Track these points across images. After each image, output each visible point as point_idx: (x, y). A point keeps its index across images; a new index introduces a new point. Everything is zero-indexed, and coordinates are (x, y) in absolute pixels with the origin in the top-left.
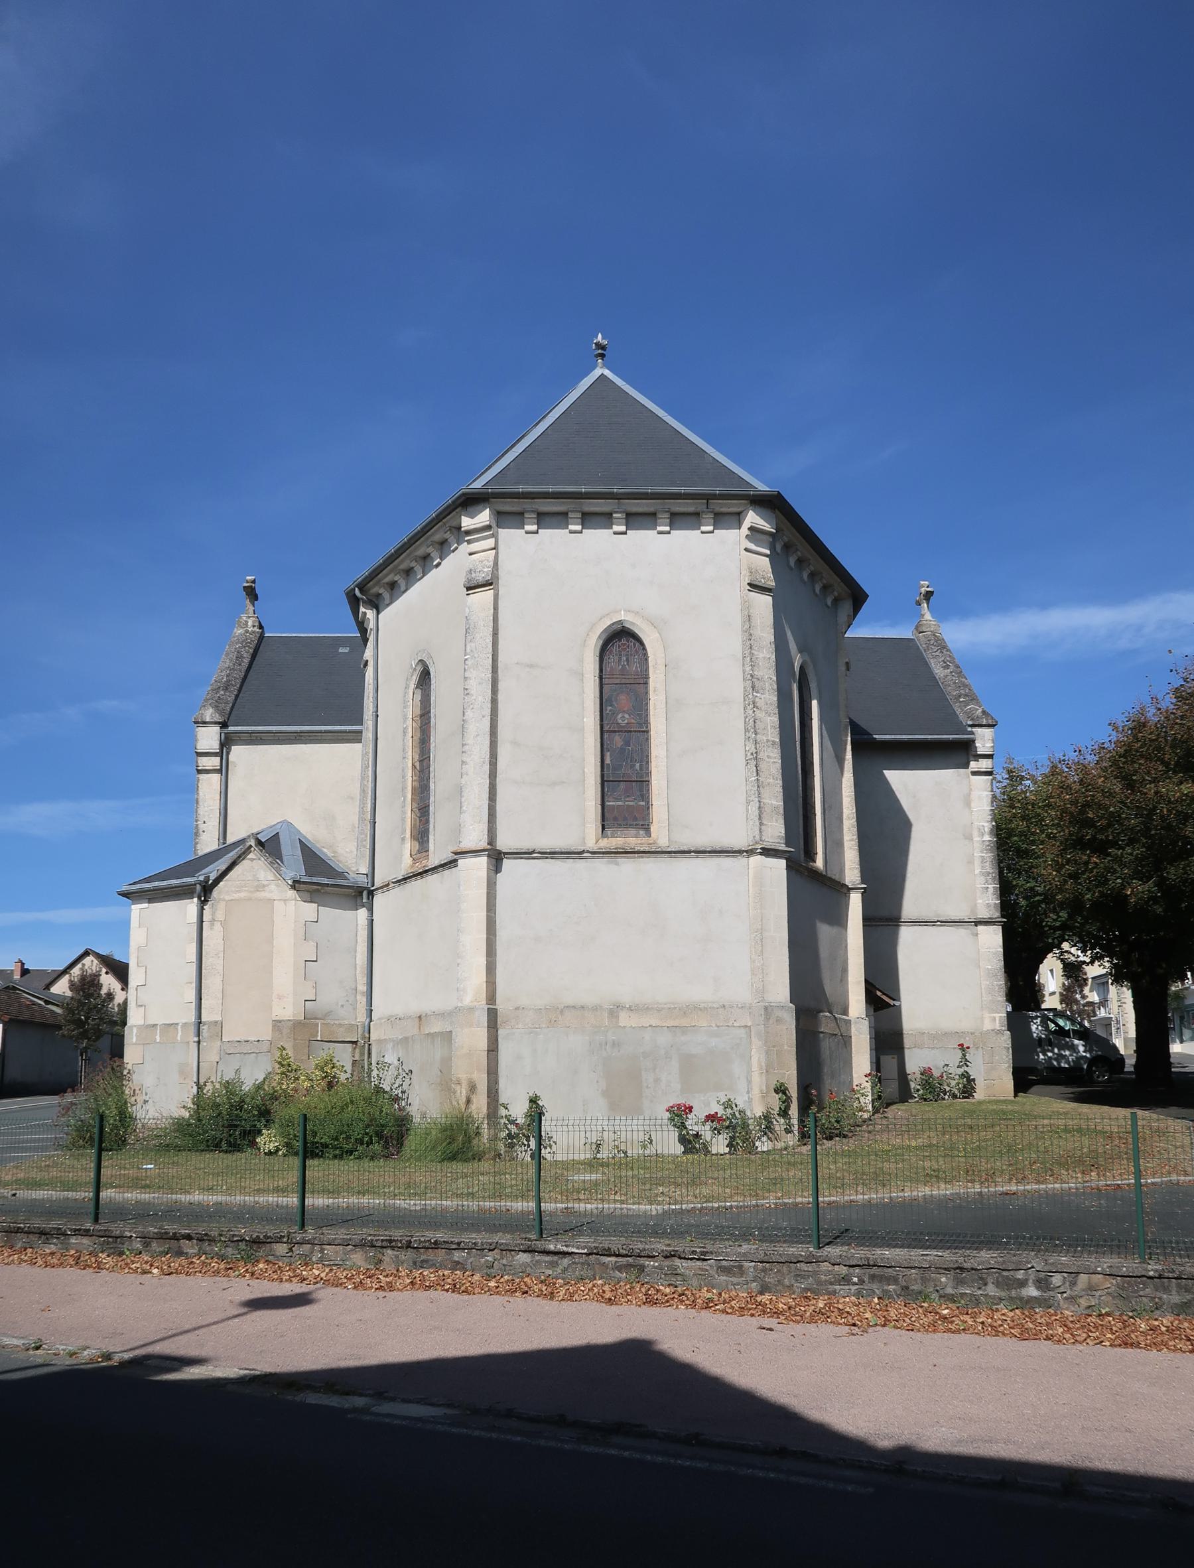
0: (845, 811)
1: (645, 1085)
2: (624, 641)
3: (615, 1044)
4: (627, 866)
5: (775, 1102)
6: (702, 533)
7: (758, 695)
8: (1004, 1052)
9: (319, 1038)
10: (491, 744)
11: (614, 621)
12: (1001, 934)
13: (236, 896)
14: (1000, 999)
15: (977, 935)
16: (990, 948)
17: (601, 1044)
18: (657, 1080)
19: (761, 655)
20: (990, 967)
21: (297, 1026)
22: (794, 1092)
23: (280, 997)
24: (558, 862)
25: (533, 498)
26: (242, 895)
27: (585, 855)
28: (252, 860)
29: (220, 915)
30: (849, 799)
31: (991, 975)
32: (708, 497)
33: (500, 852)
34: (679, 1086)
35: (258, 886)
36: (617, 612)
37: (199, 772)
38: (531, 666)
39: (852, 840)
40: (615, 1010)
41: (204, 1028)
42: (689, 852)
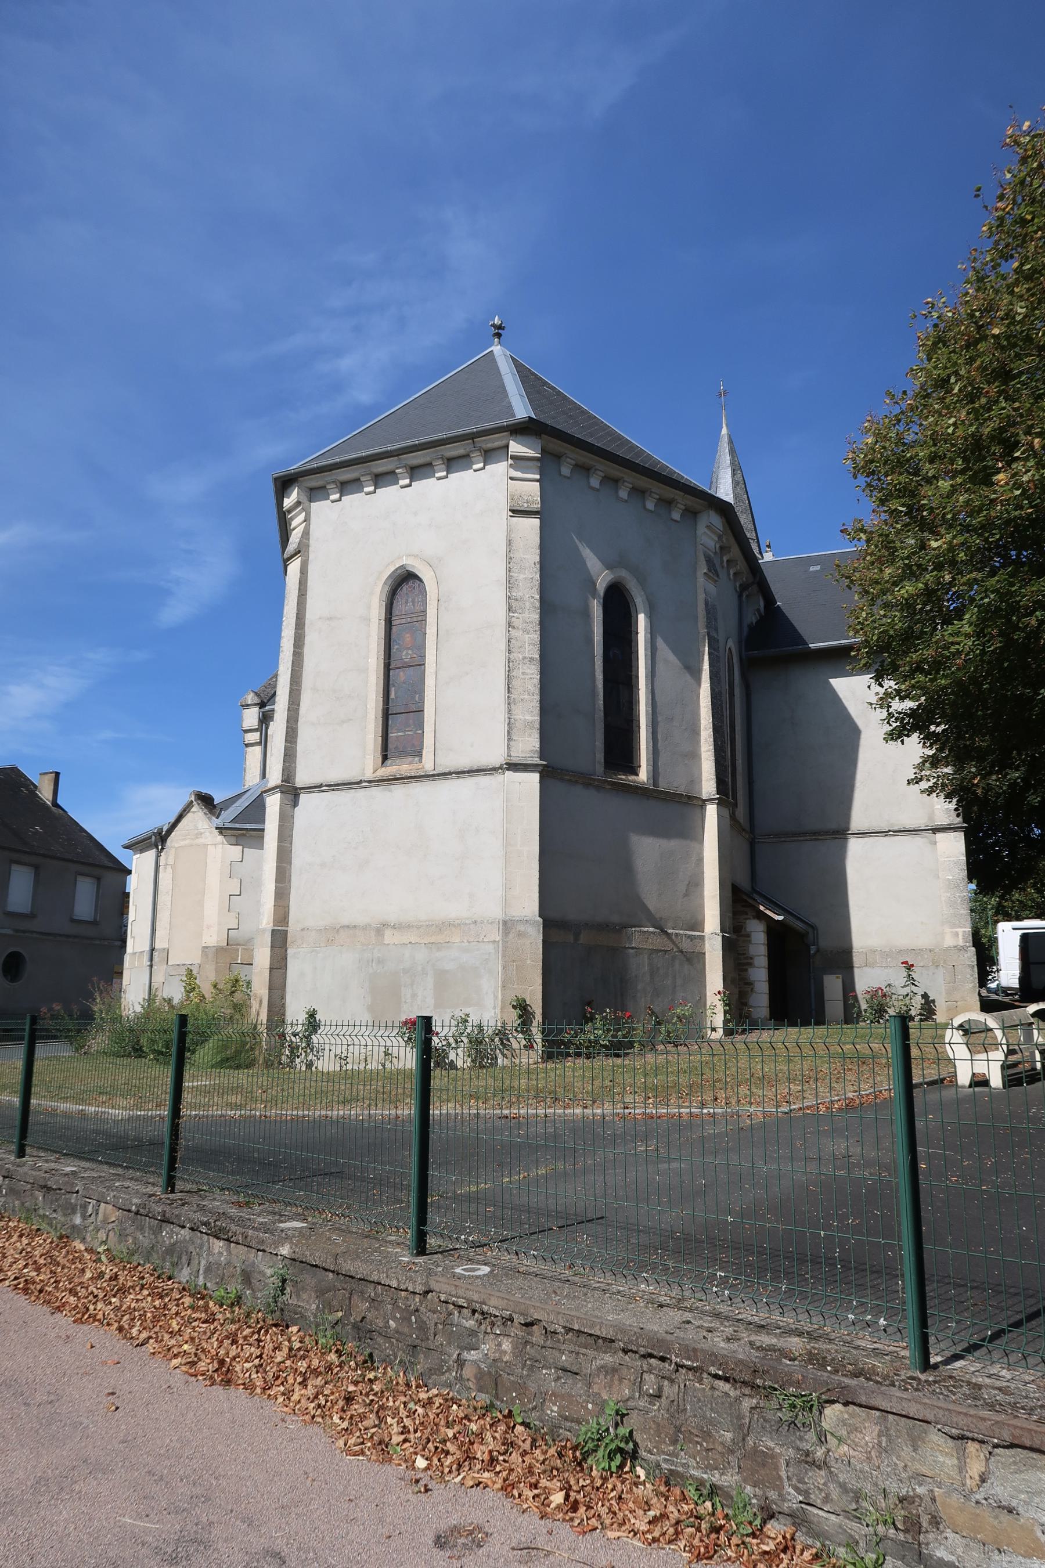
0: (702, 721)
1: (403, 1000)
2: (411, 583)
3: (380, 961)
4: (398, 791)
5: (512, 1017)
6: (475, 471)
7: (515, 615)
8: (969, 970)
9: (239, 962)
10: (290, 692)
11: (397, 566)
12: (963, 841)
13: (183, 843)
14: (962, 912)
15: (935, 843)
16: (950, 857)
17: (368, 961)
18: (414, 996)
19: (522, 576)
20: (951, 878)
21: (219, 950)
22: (537, 1008)
23: (208, 927)
24: (343, 793)
25: (330, 470)
26: (187, 842)
27: (364, 784)
28: (194, 812)
29: (171, 861)
30: (706, 710)
31: (952, 886)
32: (472, 436)
33: (296, 789)
34: (433, 1001)
35: (197, 834)
36: (400, 558)
37: (247, 745)
38: (330, 619)
39: (708, 751)
40: (381, 929)
41: (155, 954)
42: (450, 773)
